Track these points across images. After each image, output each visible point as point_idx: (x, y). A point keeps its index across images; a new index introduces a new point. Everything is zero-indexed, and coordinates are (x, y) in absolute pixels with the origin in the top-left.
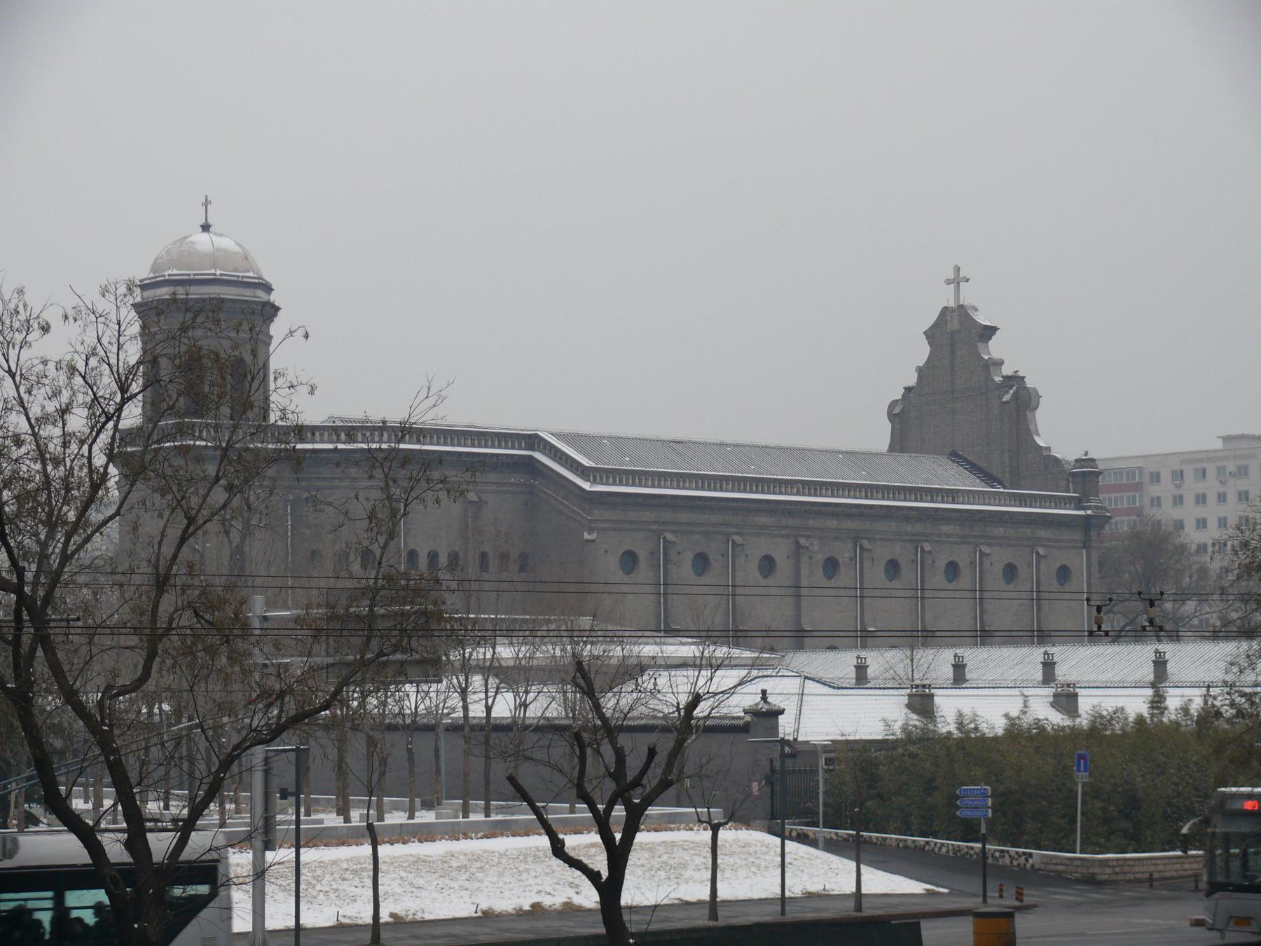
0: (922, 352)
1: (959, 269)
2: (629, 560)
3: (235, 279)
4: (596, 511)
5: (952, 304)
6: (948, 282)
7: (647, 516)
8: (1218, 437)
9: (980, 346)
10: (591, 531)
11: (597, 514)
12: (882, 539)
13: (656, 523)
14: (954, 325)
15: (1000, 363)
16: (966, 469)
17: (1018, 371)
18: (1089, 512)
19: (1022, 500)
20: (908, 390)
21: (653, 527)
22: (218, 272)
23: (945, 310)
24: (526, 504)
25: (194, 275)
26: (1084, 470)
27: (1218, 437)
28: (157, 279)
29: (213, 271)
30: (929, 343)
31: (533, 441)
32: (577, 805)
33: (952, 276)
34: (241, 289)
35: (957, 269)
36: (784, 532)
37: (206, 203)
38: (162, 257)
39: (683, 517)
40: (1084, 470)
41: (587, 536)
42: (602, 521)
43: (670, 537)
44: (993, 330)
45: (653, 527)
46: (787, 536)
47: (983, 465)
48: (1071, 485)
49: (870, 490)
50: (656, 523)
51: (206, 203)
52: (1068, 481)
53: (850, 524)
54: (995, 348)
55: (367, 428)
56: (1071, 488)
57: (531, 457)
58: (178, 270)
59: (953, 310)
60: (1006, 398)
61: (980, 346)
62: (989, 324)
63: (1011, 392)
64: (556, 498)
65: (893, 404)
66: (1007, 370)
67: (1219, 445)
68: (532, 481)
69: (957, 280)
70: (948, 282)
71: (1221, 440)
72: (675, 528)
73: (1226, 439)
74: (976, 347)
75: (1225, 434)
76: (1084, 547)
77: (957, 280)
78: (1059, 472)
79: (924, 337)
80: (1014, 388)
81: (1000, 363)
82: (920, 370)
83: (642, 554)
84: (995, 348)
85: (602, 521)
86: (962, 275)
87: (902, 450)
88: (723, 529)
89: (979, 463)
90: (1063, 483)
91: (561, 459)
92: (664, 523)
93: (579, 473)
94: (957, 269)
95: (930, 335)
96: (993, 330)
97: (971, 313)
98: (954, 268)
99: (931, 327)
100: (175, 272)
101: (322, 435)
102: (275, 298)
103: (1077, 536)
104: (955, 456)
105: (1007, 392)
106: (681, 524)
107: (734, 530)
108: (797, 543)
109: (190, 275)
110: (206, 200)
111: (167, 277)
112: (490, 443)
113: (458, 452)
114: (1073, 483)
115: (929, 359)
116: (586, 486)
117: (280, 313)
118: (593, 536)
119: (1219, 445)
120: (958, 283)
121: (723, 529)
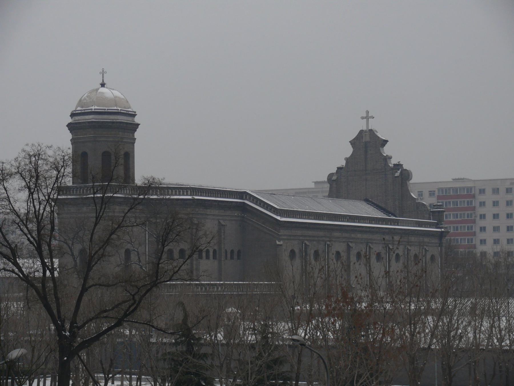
0: (349, 151)
1: (368, 112)
2: (292, 253)
3: (125, 112)
4: (281, 231)
5: (365, 128)
6: (363, 118)
7: (299, 232)
8: (313, 182)
9: (381, 149)
10: (279, 240)
11: (282, 232)
12: (375, 243)
13: (302, 236)
14: (367, 138)
15: (390, 158)
16: (375, 207)
17: (400, 162)
18: (443, 230)
19: (420, 224)
20: (339, 169)
21: (301, 238)
22: (120, 109)
23: (361, 132)
24: (240, 226)
25: (107, 109)
26: (439, 210)
27: (313, 182)
28: (86, 111)
29: (115, 108)
30: (352, 147)
31: (242, 195)
32: (299, 382)
33: (365, 115)
34: (128, 117)
35: (368, 112)
36: (344, 240)
37: (103, 73)
38: (85, 99)
39: (310, 233)
40: (439, 210)
41: (278, 243)
42: (285, 235)
43: (307, 243)
44: (386, 141)
45: (301, 238)
46: (344, 242)
47: (383, 205)
48: (431, 216)
49: (308, 215)
50: (302, 236)
51: (103, 73)
52: (430, 215)
53: (365, 236)
54: (387, 151)
55: (170, 188)
56: (432, 218)
57: (244, 203)
58: (97, 106)
59: (366, 132)
60: (397, 174)
61: (381, 149)
62: (385, 139)
63: (399, 172)
64: (258, 224)
65: (331, 176)
66: (394, 161)
67: (313, 186)
68: (243, 215)
69: (367, 117)
70: (363, 118)
71: (314, 183)
72: (308, 238)
73: (316, 183)
74: (379, 150)
75: (315, 181)
76: (439, 246)
77: (367, 117)
78: (425, 210)
79: (67, 128)
80: (400, 170)
81: (390, 158)
82: (347, 160)
83: (297, 251)
84: (387, 151)
85: (285, 235)
86: (370, 115)
87: (338, 197)
88: (324, 238)
89: (380, 205)
90: (427, 216)
91: (264, 206)
92: (305, 236)
93: (276, 213)
94: (368, 112)
95: (353, 143)
96: (386, 141)
97: (375, 133)
98: (366, 112)
99: (354, 139)
100: (96, 107)
101: (172, 191)
102: (137, 120)
103: (436, 241)
104: (367, 201)
105: (397, 172)
106: (310, 236)
107: (328, 239)
108: (348, 245)
109: (105, 109)
110: (103, 71)
111: (93, 110)
112: (185, 193)
113: (218, 200)
114: (432, 216)
115: (352, 154)
116: (279, 218)
117: (66, 125)
118: (281, 243)
119: (313, 186)
120: (368, 119)
121: (324, 238)
